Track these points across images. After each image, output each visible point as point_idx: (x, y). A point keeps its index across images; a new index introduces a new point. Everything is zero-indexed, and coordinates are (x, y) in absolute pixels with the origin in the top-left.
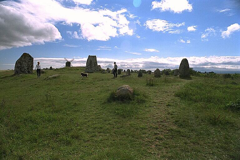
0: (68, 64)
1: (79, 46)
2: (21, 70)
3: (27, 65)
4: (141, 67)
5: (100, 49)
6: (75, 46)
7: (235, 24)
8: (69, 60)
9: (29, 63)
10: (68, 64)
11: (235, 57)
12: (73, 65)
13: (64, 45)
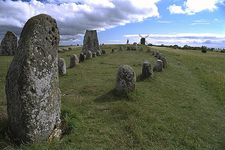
0: (143, 40)
1: (172, 22)
2: (6, 51)
3: (11, 45)
4: (199, 43)
5: (195, 24)
6: (168, 22)
7: (157, 7)
8: (144, 36)
9: (13, 43)
10: (143, 40)
11: (177, 33)
12: (148, 41)
13: (158, 22)
